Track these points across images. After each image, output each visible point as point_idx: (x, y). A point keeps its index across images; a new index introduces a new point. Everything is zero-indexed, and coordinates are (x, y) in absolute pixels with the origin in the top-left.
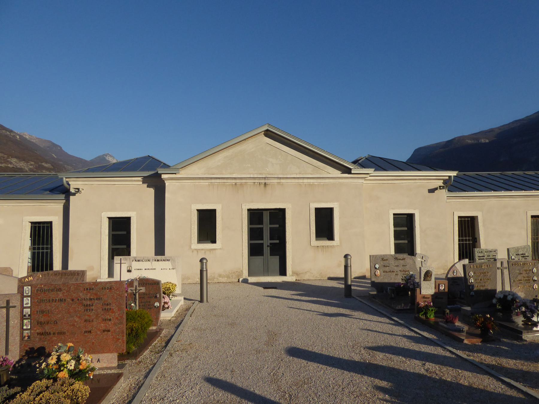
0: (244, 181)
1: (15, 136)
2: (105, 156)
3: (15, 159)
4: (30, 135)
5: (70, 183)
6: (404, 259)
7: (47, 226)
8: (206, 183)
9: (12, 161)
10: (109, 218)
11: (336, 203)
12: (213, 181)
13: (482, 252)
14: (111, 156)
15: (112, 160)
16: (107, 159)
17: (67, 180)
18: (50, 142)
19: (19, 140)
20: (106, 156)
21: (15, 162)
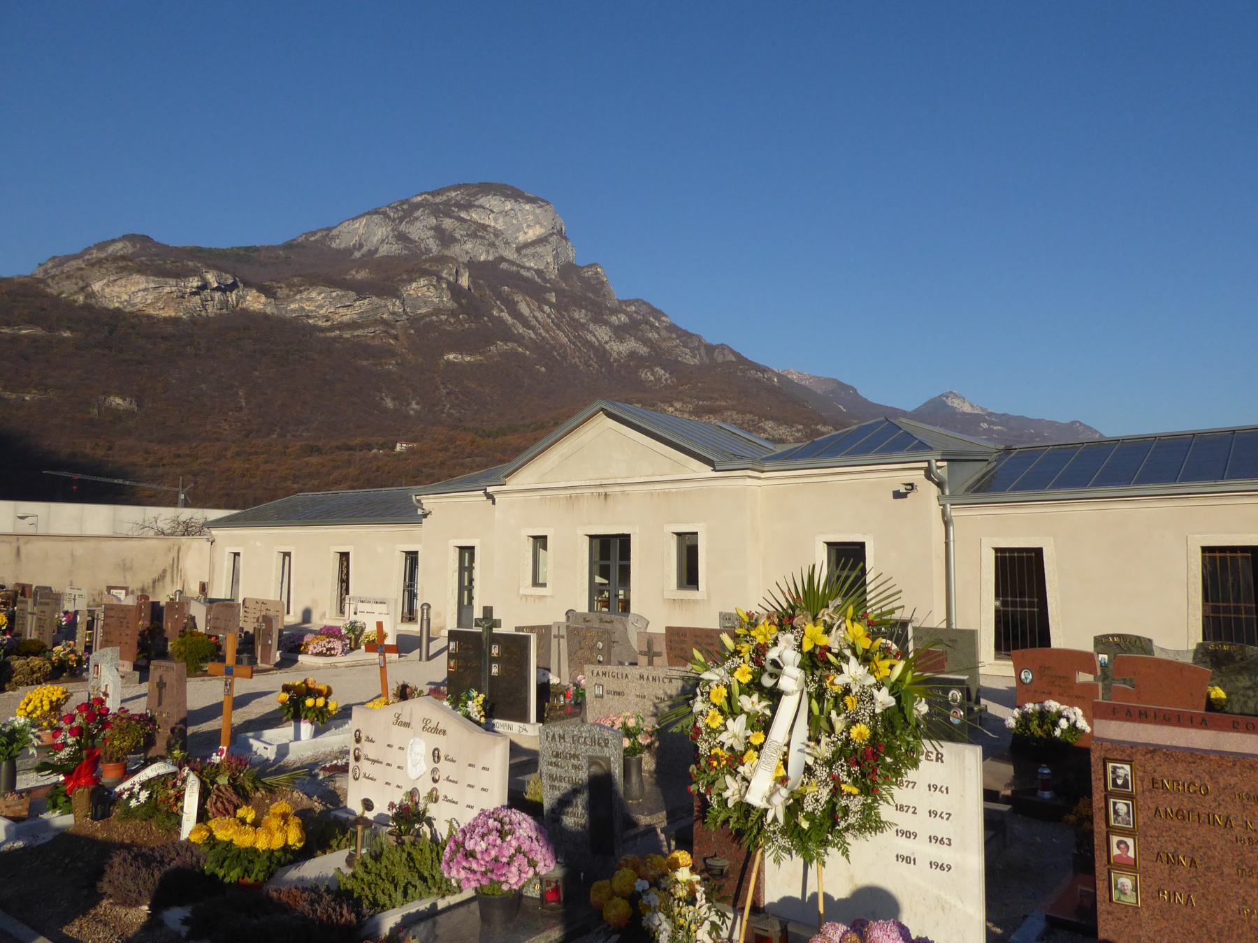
0: (578, 491)
1: (770, 378)
2: (944, 399)
3: (771, 422)
4: (799, 373)
5: (423, 501)
6: (611, 622)
7: (1220, 557)
8: (536, 495)
9: (766, 427)
10: (829, 544)
11: (701, 525)
12: (545, 493)
13: (730, 619)
14: (956, 396)
15: (961, 404)
16: (950, 404)
17: (418, 497)
18: (835, 381)
19: (777, 385)
20: (947, 397)
21: (772, 428)
